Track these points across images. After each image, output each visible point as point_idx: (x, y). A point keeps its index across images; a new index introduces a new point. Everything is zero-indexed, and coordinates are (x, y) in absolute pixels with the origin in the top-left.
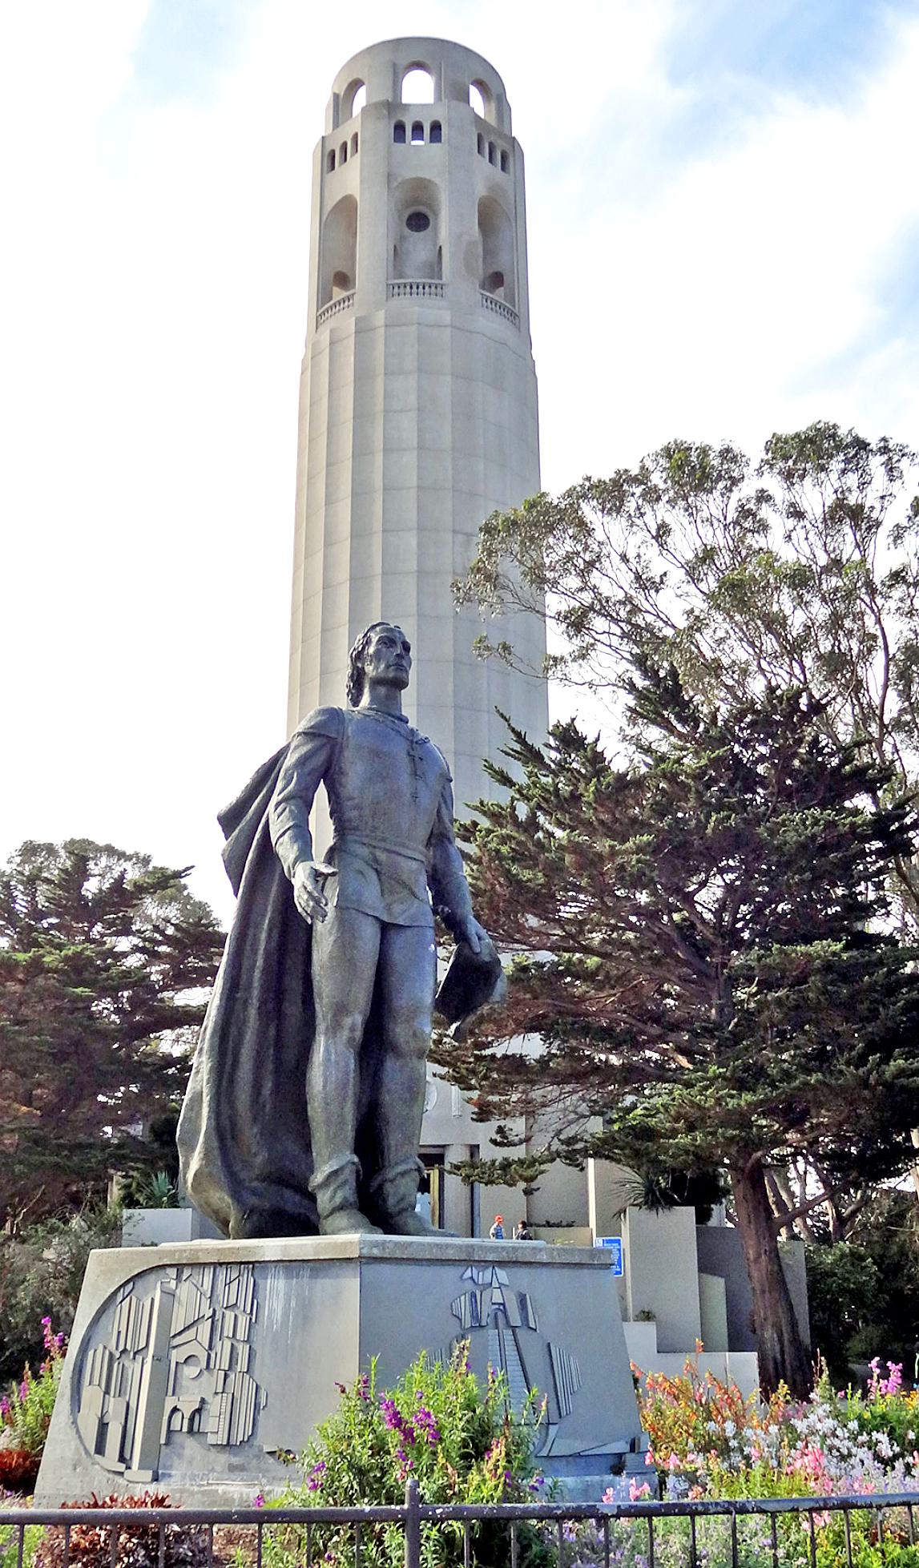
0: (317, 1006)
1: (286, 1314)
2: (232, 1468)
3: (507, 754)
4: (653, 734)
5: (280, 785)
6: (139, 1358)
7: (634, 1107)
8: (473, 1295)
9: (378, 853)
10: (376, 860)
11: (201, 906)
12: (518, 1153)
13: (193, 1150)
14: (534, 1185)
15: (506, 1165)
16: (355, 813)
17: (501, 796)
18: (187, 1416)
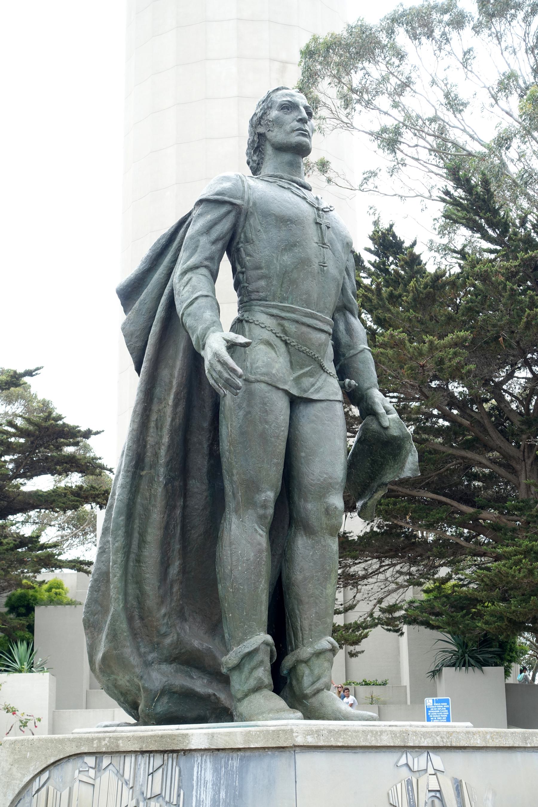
0: (227, 484)
4: (462, 236)
5: (183, 255)
7: (449, 578)
8: (409, 783)
9: (286, 324)
10: (285, 331)
11: (45, 404)
13: (100, 630)
14: (358, 648)
16: (263, 283)
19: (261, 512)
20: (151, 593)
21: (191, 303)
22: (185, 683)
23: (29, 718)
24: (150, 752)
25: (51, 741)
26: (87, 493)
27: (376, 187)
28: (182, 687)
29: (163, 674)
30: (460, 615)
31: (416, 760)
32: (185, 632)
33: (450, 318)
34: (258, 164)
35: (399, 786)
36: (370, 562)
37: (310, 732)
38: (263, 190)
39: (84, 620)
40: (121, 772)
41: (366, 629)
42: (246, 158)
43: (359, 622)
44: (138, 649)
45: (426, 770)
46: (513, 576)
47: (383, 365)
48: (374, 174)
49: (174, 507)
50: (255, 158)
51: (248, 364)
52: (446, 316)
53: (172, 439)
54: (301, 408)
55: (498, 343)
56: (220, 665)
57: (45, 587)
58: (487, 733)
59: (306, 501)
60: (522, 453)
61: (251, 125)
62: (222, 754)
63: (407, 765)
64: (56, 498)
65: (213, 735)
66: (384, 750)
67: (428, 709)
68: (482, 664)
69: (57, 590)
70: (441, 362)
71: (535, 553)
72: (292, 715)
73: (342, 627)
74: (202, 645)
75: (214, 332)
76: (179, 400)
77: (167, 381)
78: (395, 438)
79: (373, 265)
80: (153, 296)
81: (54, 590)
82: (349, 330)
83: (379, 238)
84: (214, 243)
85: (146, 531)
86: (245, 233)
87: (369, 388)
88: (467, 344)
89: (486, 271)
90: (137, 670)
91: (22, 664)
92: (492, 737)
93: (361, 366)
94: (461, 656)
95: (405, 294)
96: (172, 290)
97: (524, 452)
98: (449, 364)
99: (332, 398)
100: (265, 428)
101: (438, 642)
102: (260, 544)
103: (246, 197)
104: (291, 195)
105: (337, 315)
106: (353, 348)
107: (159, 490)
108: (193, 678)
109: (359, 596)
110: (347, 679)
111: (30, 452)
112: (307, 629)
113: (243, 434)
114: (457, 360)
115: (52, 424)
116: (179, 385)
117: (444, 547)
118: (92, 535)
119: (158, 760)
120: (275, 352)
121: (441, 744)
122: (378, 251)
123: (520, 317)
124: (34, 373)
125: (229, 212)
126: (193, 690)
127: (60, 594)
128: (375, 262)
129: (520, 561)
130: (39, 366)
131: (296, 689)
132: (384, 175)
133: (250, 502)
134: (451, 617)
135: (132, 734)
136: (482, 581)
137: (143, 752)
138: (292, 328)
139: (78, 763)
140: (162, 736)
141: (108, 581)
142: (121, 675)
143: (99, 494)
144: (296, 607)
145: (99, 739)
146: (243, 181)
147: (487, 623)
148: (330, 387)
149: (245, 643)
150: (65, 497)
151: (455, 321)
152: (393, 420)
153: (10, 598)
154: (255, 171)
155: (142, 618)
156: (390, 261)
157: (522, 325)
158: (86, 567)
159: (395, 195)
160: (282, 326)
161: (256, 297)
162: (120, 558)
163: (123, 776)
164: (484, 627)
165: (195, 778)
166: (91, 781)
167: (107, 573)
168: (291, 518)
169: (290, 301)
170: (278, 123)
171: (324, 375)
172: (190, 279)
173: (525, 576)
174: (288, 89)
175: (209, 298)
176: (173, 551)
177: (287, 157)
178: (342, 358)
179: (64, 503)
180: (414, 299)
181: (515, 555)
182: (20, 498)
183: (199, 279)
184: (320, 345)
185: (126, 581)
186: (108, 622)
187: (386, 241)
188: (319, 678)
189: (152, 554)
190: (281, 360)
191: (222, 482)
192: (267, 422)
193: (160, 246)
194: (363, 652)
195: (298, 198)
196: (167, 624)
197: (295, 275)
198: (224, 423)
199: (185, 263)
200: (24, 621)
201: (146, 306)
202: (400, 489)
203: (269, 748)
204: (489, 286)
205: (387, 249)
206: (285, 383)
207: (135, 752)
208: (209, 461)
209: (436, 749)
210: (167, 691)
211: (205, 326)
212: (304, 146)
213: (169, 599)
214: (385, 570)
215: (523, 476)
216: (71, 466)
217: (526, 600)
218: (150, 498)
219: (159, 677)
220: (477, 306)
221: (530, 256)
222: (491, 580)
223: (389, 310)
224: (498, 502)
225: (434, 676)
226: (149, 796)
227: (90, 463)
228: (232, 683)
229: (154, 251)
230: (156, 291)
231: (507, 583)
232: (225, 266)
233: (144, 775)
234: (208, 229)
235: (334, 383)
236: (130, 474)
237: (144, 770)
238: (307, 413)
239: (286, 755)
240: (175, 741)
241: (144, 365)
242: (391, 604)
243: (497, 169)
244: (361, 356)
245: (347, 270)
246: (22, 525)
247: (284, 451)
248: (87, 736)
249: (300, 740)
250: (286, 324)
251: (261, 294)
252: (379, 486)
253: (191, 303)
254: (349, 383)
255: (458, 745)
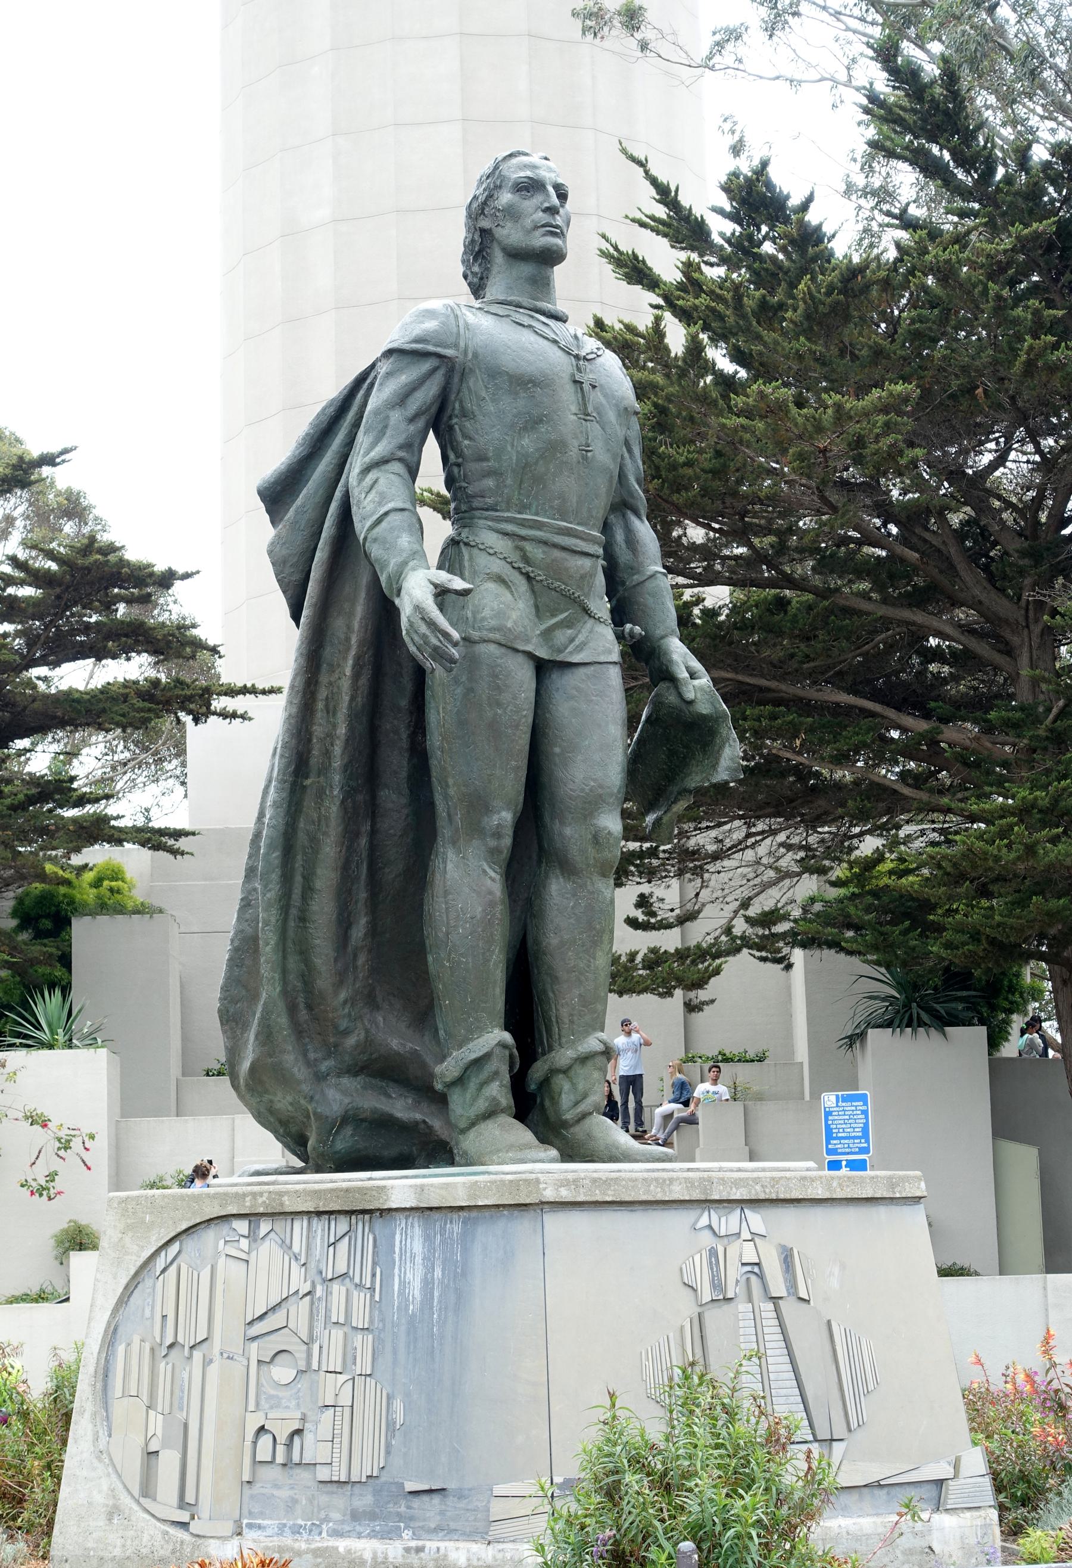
1: (427, 1284)
2: (355, 1516)
3: (643, 225)
5: (363, 439)
6: (197, 1354)
7: (879, 857)
8: (713, 1252)
9: (528, 547)
10: (526, 559)
12: (669, 941)
13: (246, 1027)
14: (703, 995)
15: (655, 959)
17: (637, 307)
18: (282, 1438)
19: (492, 843)
20: (323, 969)
21: (379, 521)
22: (378, 1106)
23: (73, 1133)
24: (330, 1213)
25: (182, 1198)
26: (169, 694)
27: (740, 61)
28: (374, 1111)
29: (345, 1092)
30: (897, 930)
31: (723, 1219)
32: (377, 1027)
33: (878, 353)
34: (481, 278)
35: (697, 1258)
36: (727, 827)
37: (565, 1183)
38: (488, 328)
39: (220, 1011)
40: (288, 1241)
41: (718, 957)
42: (461, 269)
43: (704, 945)
44: (305, 1054)
45: (739, 1234)
46: (997, 859)
47: (748, 447)
48: (734, 35)
49: (358, 835)
50: (476, 269)
51: (470, 615)
52: (870, 347)
53: (351, 728)
54: (554, 676)
55: (974, 397)
56: (432, 1075)
57: (89, 876)
58: (833, 1178)
59: (562, 823)
60: (1023, 612)
61: (469, 216)
62: (436, 1215)
63: (710, 1227)
64: (108, 705)
65: (422, 1188)
66: (675, 1206)
67: (828, 1114)
68: (944, 1021)
69: (113, 884)
70: (859, 442)
71: (1040, 811)
72: (542, 1155)
73: (672, 955)
74: (404, 1045)
75: (414, 569)
76: (361, 667)
77: (342, 636)
78: (704, 718)
79: (728, 241)
80: (317, 500)
81: (106, 883)
82: (632, 541)
83: (740, 187)
84: (412, 420)
85: (314, 873)
86: (461, 402)
87: (663, 637)
88: (909, 408)
89: (948, 261)
90: (305, 1088)
91: (53, 1032)
92: (840, 1185)
93: (650, 601)
94: (904, 1006)
95: (790, 302)
96: (347, 492)
97: (1027, 610)
98: (874, 446)
99: (602, 659)
100: (496, 714)
101: (857, 980)
102: (490, 893)
103: (462, 344)
104: (533, 337)
105: (612, 518)
106: (638, 572)
107: (333, 809)
108: (390, 1097)
109: (705, 895)
110: (687, 1051)
111: (56, 614)
112: (566, 1021)
113: (462, 723)
114: (889, 440)
115: (96, 561)
116: (361, 644)
117: (869, 799)
118: (175, 762)
119: (342, 1225)
120: (512, 592)
121: (762, 1196)
122: (738, 213)
123: (1014, 352)
124: (58, 460)
125: (435, 370)
126: (391, 1116)
127: (119, 892)
128: (733, 234)
129: (1011, 827)
130: (69, 446)
131: (550, 1112)
132: (756, 36)
133: (475, 829)
134: (882, 934)
135: (302, 1186)
136: (939, 866)
137: (319, 1214)
138: (536, 552)
139: (224, 1229)
140: (347, 1190)
141: (256, 951)
142: (280, 1095)
143: (192, 696)
144: (548, 986)
145: (254, 1195)
146: (456, 317)
147: (948, 945)
148: (601, 642)
149: (470, 1046)
150: (125, 701)
151: (888, 357)
152: (701, 689)
153: (20, 901)
154: (477, 290)
155: (310, 1007)
156: (763, 232)
157: (1018, 366)
158: (171, 842)
159: (778, 78)
160: (521, 549)
161: (480, 505)
162: (274, 916)
163: (291, 1248)
164: (944, 953)
165: (397, 1250)
166: (244, 1256)
167: (255, 939)
168: (541, 848)
169: (533, 510)
170: (512, 213)
171: (591, 621)
172: (376, 482)
173: (1019, 858)
174: (526, 154)
175: (406, 513)
176: (356, 902)
177: (527, 269)
178: (620, 588)
179: (123, 715)
180: (808, 317)
181: (1002, 817)
182: (36, 705)
183: (389, 480)
184: (583, 577)
185: (284, 951)
186: (258, 1015)
187: (754, 194)
188: (585, 1096)
189: (323, 908)
190: (521, 605)
191: (431, 792)
192: (499, 704)
193: (325, 419)
194: (713, 1001)
195: (546, 342)
196: (350, 1015)
197: (541, 468)
198: (433, 705)
199: (367, 453)
200: (52, 948)
201: (307, 516)
202: (783, 687)
203: (504, 1206)
204: (954, 289)
205: (757, 210)
206: (528, 641)
207: (308, 1213)
208: (410, 760)
209: (755, 1203)
210: (350, 1118)
211: (400, 559)
212: (555, 252)
213: (351, 977)
214: (757, 842)
215: (1024, 659)
216: (137, 642)
217: (1022, 903)
218: (319, 821)
219: (338, 1096)
220: (930, 329)
221: (1035, 232)
222: (955, 865)
223: (759, 337)
224: (974, 707)
225: (851, 1046)
226: (330, 1276)
227: (173, 635)
228: (452, 1106)
229: (316, 426)
230: (321, 492)
231: (986, 870)
232: (432, 447)
233: (322, 1247)
234: (402, 398)
235: (607, 633)
236: (287, 785)
237: (322, 1239)
238: (564, 683)
239: (530, 1215)
240: (367, 1197)
241: (305, 613)
242: (767, 909)
243: (973, 47)
244: (650, 585)
245: (627, 443)
246: (39, 758)
247: (527, 747)
248: (234, 1189)
249: (549, 1195)
250: (528, 547)
251: (488, 500)
252: (679, 793)
253: (379, 521)
254: (631, 630)
255: (788, 1196)
